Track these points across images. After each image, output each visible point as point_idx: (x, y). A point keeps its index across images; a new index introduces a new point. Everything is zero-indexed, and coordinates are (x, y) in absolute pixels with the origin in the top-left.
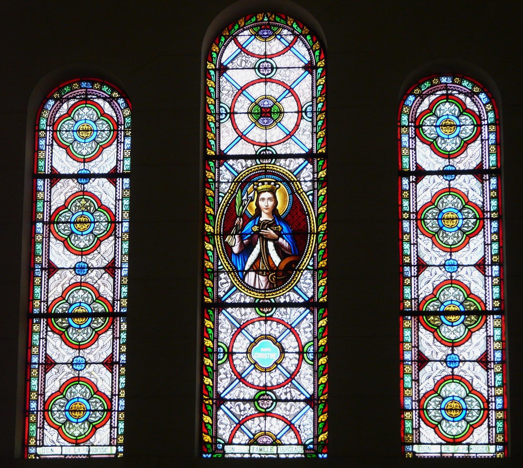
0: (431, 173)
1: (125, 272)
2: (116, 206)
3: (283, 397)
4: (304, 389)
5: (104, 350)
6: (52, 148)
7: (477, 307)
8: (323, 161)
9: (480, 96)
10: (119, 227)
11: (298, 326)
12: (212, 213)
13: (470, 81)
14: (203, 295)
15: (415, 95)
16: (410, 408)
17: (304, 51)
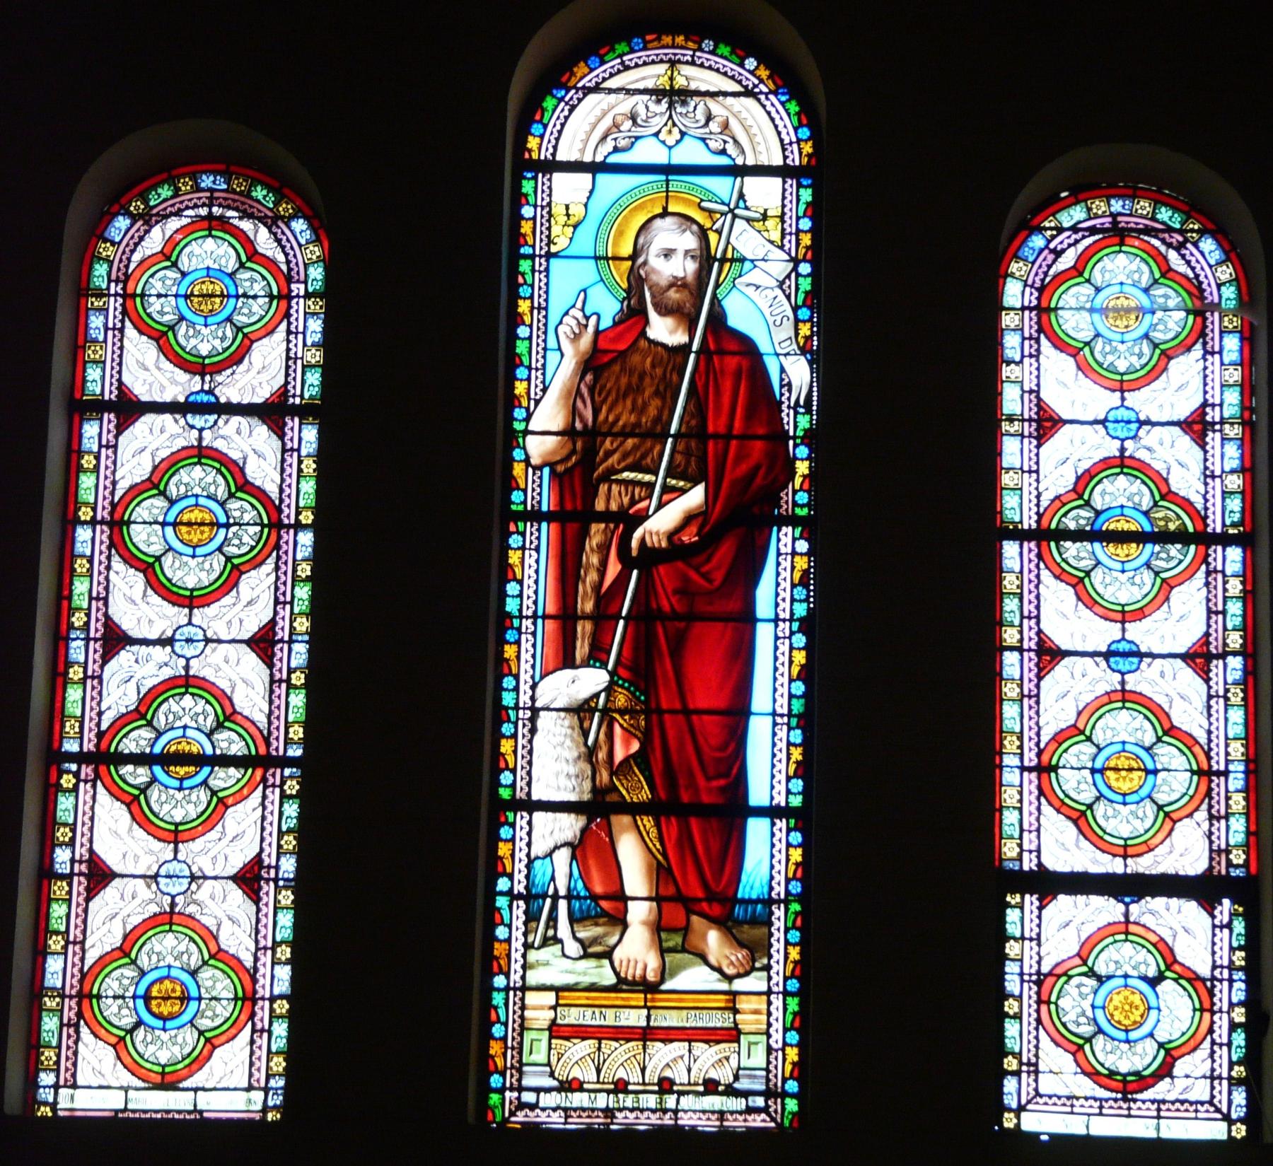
5: (264, 377)
6: (122, 336)
7: (1184, 523)
9: (294, 224)
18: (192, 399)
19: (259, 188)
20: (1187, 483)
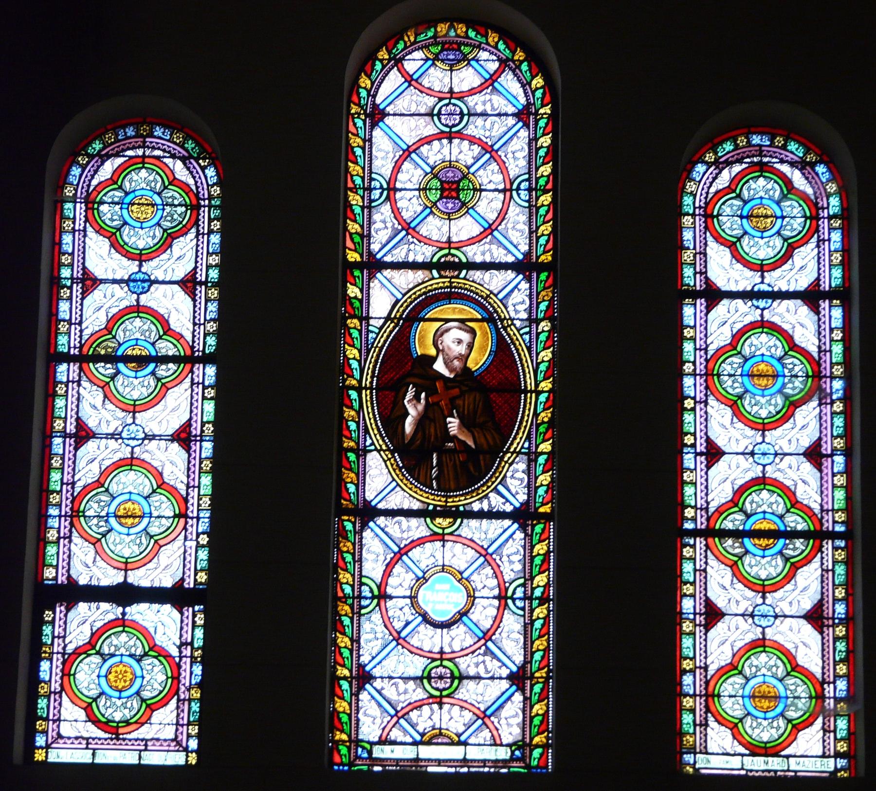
0: (732, 295)
1: (204, 525)
3: (472, 672)
4: (508, 657)
8: (542, 526)
11: (497, 713)
12: (359, 296)
13: (800, 143)
14: (341, 435)
15: (707, 163)
17: (515, 88)
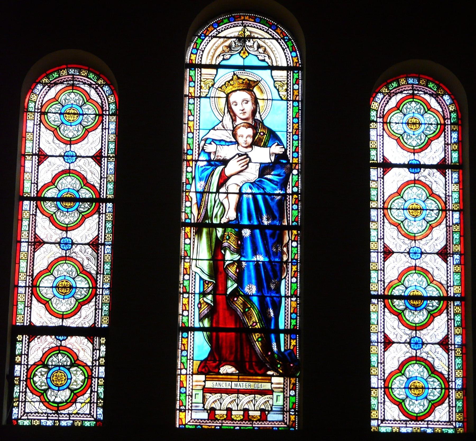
2: (101, 185)
9: (444, 97)
10: (103, 207)
16: (376, 387)
18: (410, 162)
19: (431, 83)
20: (94, 179)
